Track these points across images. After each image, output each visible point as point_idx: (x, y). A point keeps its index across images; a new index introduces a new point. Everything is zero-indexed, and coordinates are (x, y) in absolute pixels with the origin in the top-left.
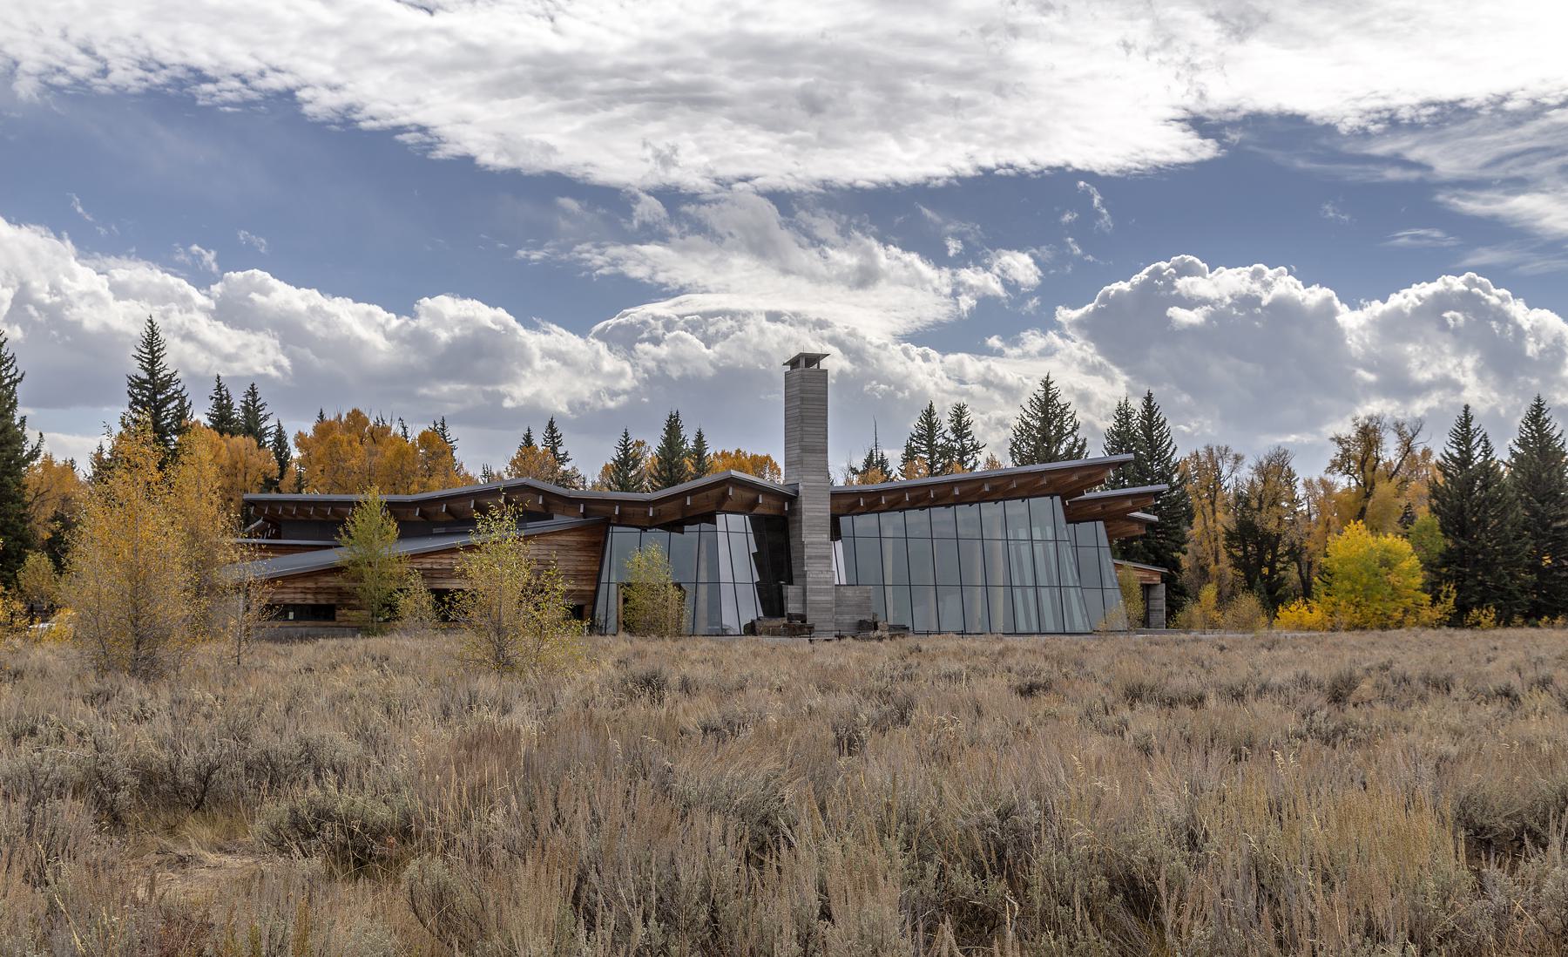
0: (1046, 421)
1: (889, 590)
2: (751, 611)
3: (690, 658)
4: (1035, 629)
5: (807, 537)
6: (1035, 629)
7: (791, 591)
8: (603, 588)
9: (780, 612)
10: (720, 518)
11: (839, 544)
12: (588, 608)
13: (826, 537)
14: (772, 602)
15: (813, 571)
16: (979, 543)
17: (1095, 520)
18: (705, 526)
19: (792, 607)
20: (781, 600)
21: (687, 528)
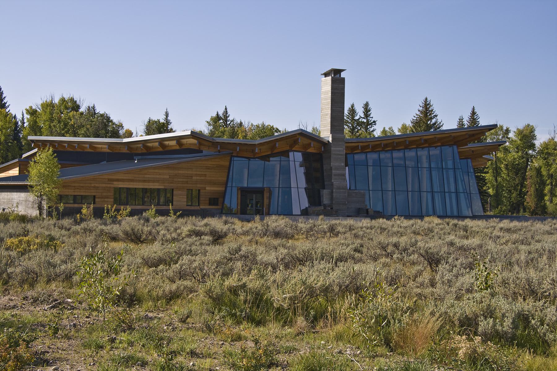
0: (427, 109)
1: (371, 192)
2: (305, 204)
3: (473, 174)
4: (455, 213)
5: (334, 164)
6: (455, 213)
7: (325, 193)
8: (229, 189)
9: (319, 203)
10: (291, 154)
11: (347, 168)
12: (221, 200)
13: (343, 164)
14: (314, 197)
15: (336, 182)
16: (435, 190)
17: (467, 158)
18: (283, 158)
19: (326, 200)
20: (319, 197)
21: (271, 159)
